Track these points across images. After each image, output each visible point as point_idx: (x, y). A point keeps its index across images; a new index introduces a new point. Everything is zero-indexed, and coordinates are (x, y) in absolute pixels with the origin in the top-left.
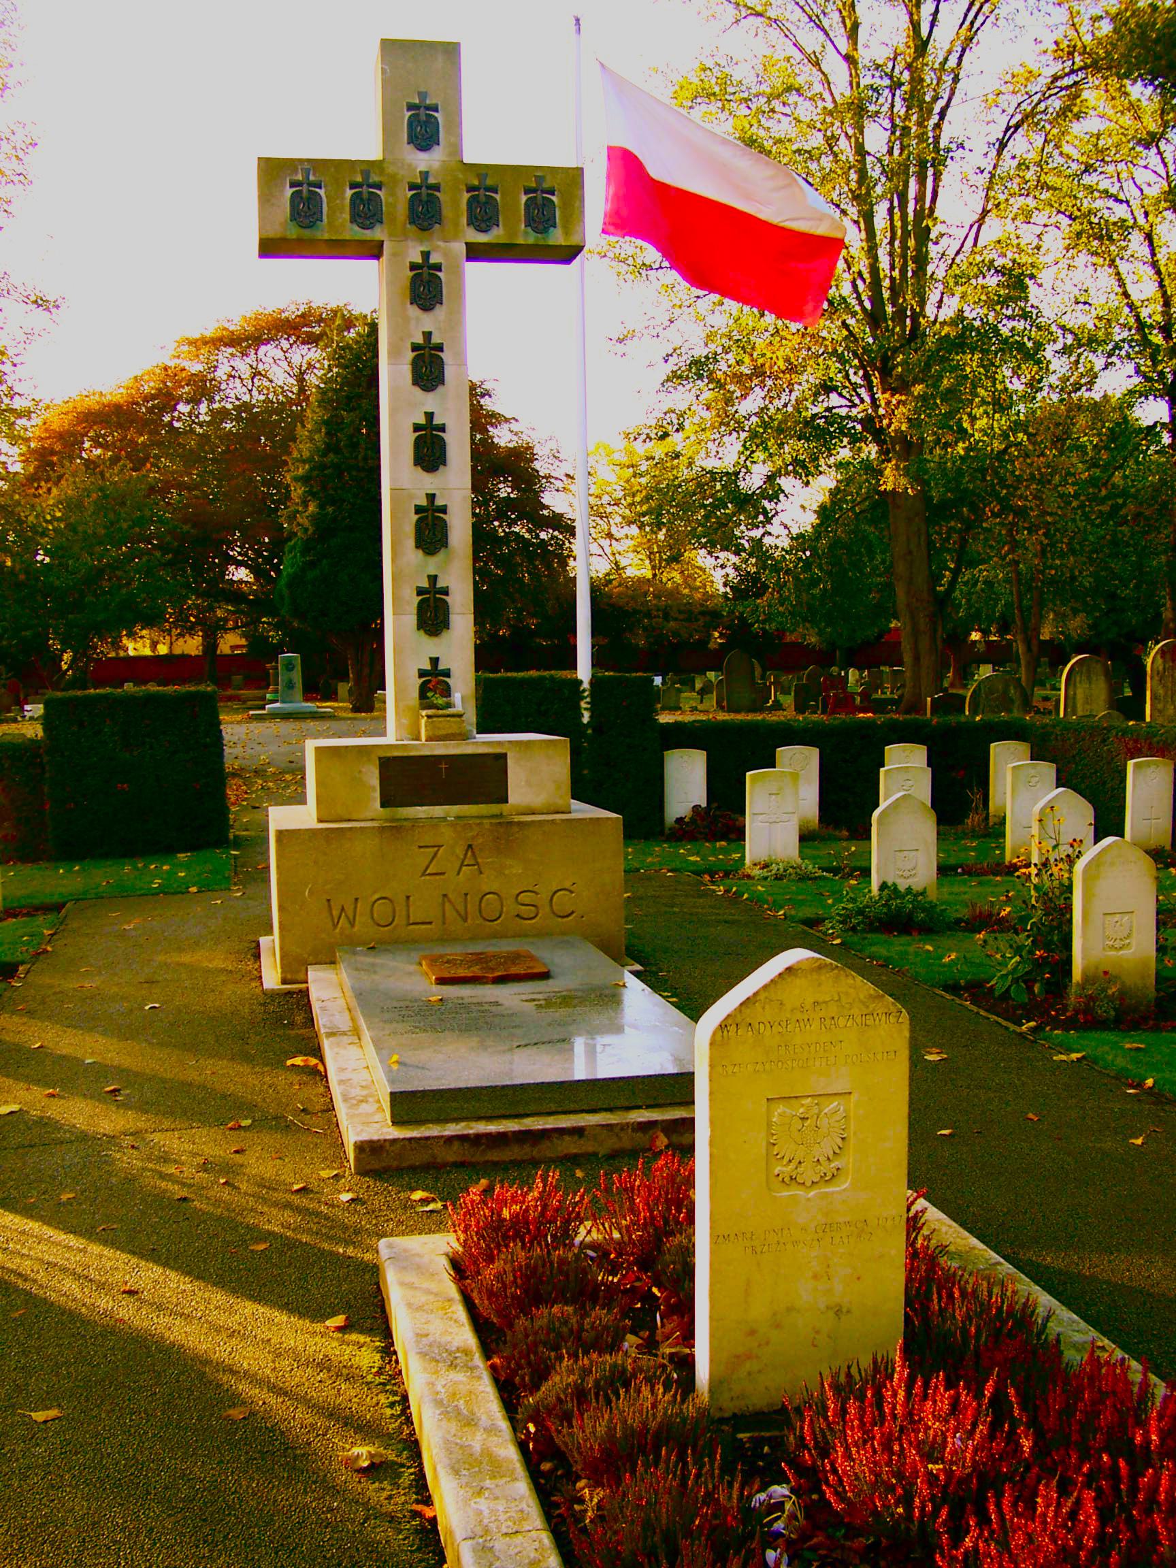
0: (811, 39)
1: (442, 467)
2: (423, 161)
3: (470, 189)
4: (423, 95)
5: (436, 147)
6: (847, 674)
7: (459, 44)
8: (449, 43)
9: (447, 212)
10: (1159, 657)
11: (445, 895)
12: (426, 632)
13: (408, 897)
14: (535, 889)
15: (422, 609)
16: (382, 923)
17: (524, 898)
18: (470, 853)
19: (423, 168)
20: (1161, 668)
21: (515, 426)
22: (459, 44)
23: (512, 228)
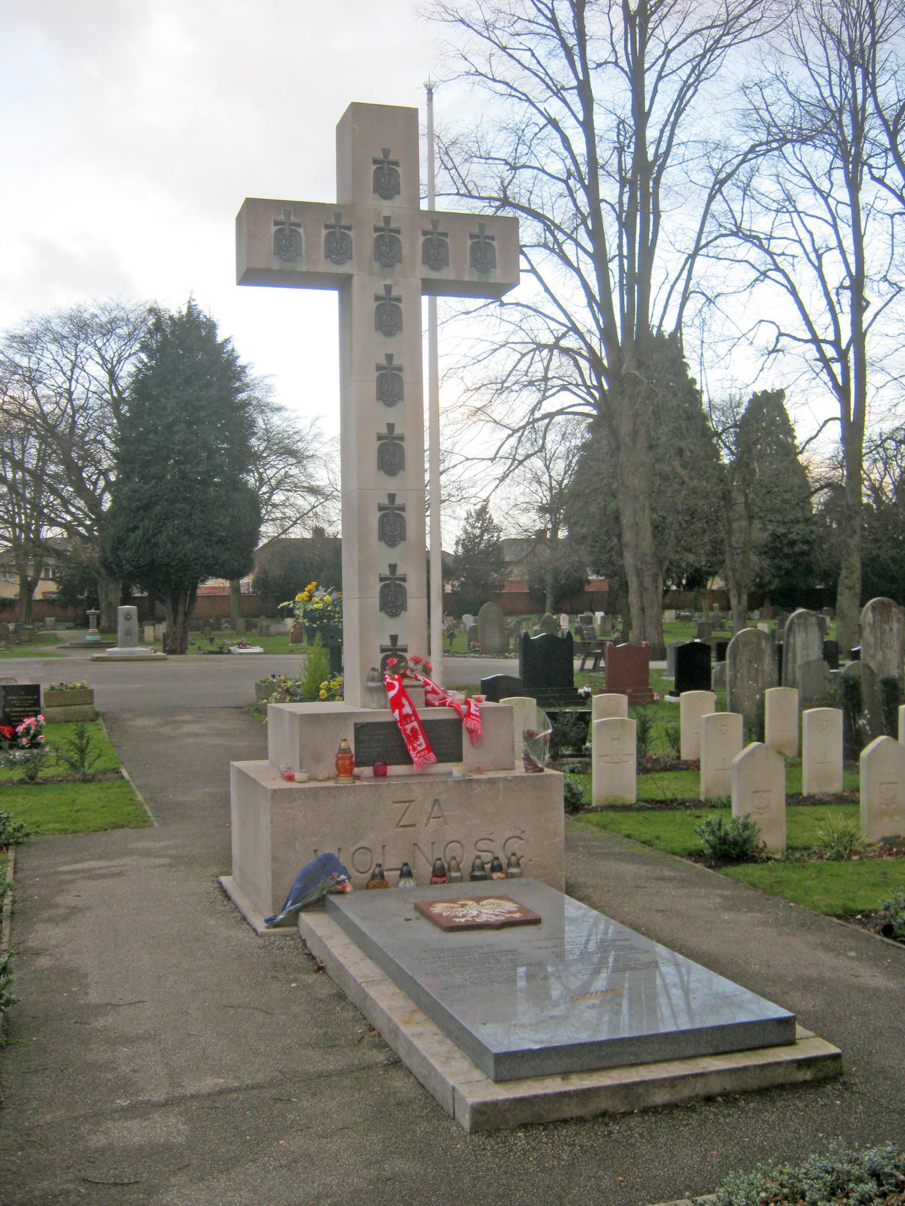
0: (555, 107)
1: (401, 472)
2: (387, 207)
3: (425, 233)
4: (386, 152)
5: (397, 196)
6: (559, 618)
7: (417, 109)
8: (409, 109)
9: (405, 252)
10: (869, 611)
11: (415, 844)
12: (387, 613)
13: (384, 847)
14: (491, 837)
15: (384, 593)
16: (361, 870)
17: (482, 845)
18: (436, 807)
19: (386, 213)
20: (871, 621)
21: (285, 414)
22: (417, 109)
23: (459, 266)
